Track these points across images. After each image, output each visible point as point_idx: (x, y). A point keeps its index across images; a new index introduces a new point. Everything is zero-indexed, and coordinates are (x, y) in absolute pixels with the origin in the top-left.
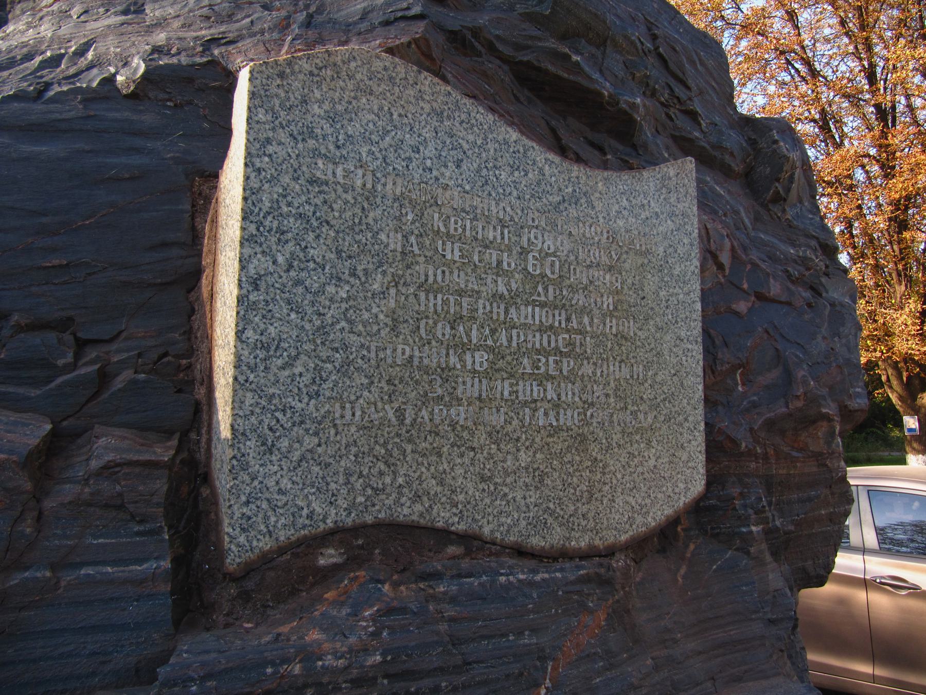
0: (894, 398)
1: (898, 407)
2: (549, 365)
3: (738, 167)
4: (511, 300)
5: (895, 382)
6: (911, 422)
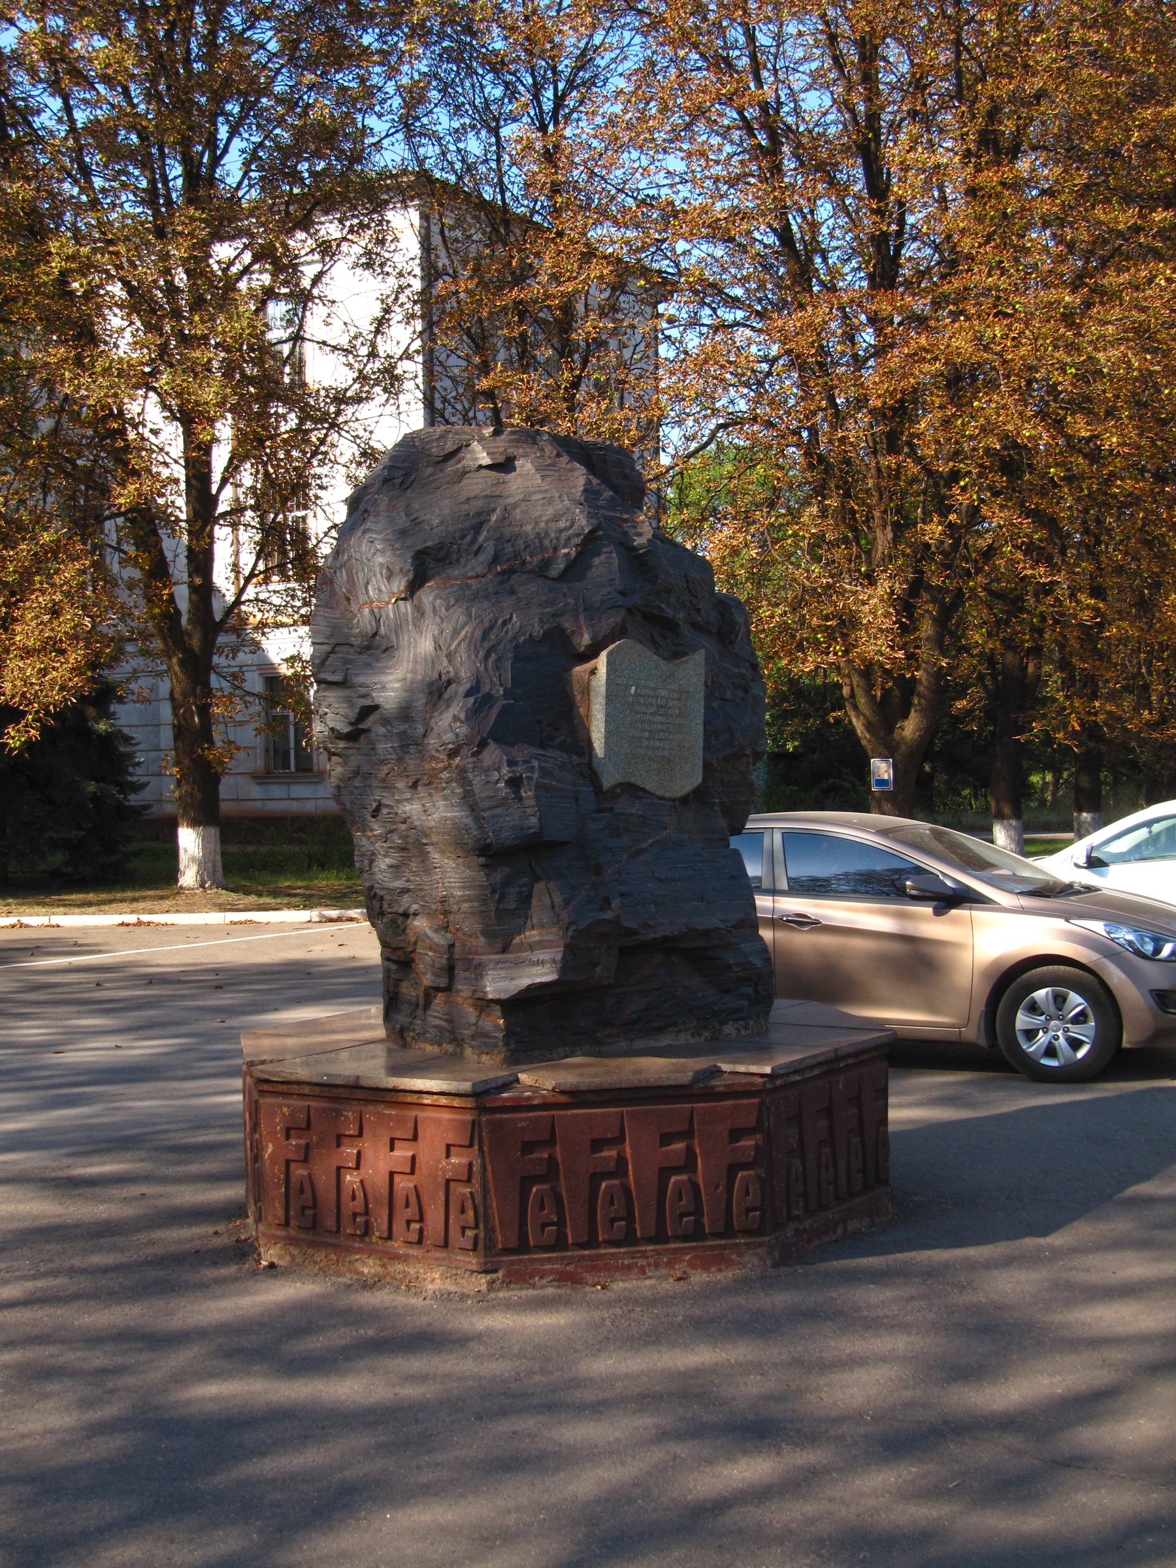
0: (858, 725)
1: (864, 742)
2: (662, 735)
3: (714, 630)
4: (653, 714)
5: (862, 700)
6: (882, 769)
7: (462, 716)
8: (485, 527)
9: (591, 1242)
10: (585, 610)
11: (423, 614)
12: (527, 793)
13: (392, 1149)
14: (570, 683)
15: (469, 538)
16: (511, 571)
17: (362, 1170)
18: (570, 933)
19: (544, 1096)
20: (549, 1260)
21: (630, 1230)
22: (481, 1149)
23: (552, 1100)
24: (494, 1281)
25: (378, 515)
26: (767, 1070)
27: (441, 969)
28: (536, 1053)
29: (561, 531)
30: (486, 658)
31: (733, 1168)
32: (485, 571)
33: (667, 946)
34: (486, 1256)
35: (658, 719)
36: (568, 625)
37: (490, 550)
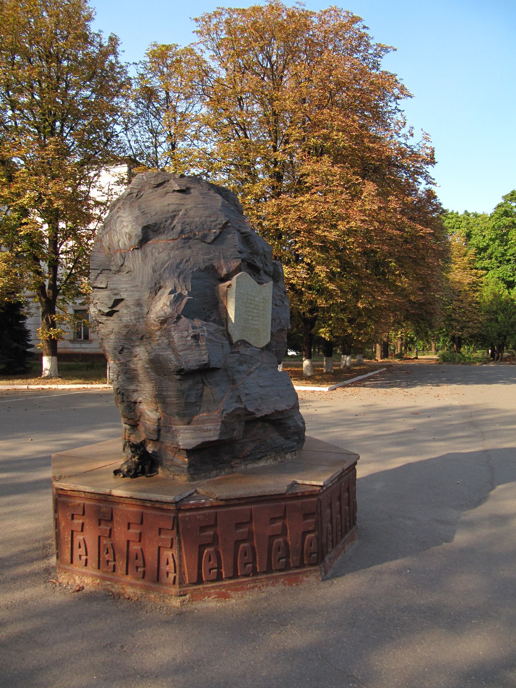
3: (272, 274)
4: (253, 309)
7: (168, 303)
8: (177, 218)
9: (235, 576)
10: (224, 258)
11: (146, 256)
12: (202, 343)
13: (129, 528)
14: (218, 292)
15: (169, 222)
16: (189, 238)
17: (112, 538)
18: (224, 415)
19: (211, 502)
20: (213, 587)
21: (254, 568)
22: (178, 531)
23: (216, 504)
24: (184, 601)
25: (125, 209)
26: (322, 484)
27: (154, 431)
28: (203, 474)
29: (212, 222)
30: (179, 277)
31: (305, 533)
32: (177, 237)
33: (265, 419)
34: (180, 587)
35: (255, 311)
36: (216, 264)
37: (179, 228)
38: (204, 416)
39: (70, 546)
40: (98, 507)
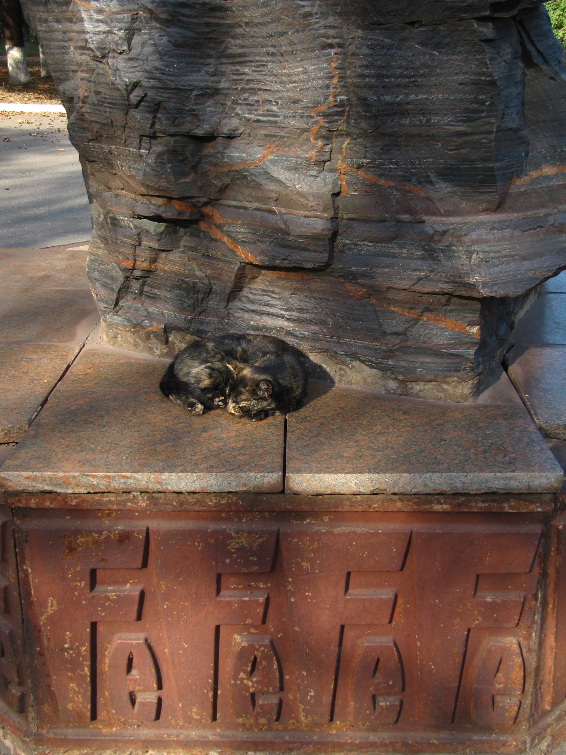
38: (547, 178)
39: (87, 671)
40: (215, 534)
